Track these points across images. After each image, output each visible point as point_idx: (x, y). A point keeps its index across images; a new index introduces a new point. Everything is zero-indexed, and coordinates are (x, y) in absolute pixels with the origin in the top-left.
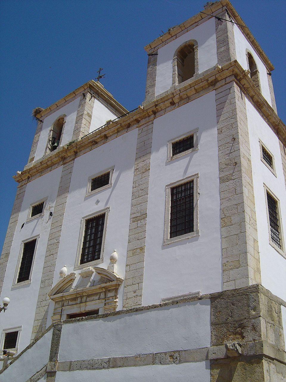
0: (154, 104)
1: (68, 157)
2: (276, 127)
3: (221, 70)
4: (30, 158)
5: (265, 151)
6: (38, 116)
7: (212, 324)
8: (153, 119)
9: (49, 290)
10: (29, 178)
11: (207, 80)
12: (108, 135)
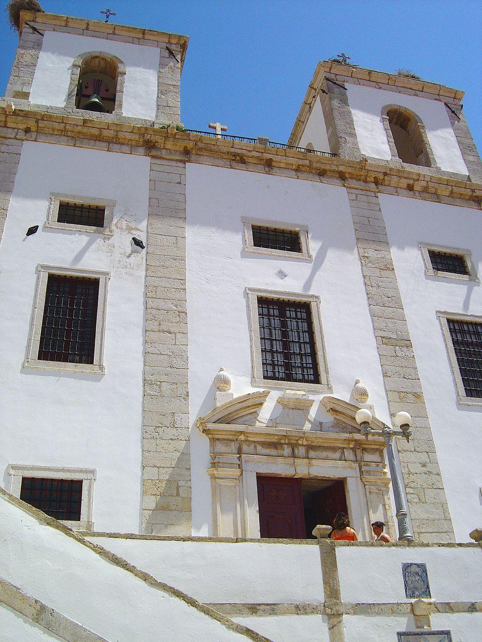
0: (384, 171)
10: (27, 131)
11: (473, 191)
12: (274, 164)
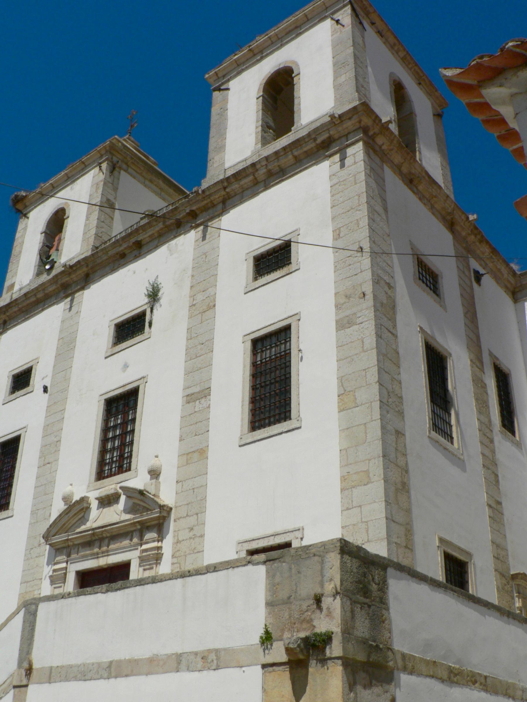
1: (73, 283)
2: (449, 218)
3: (339, 121)
4: (7, 284)
5: (423, 264)
6: (19, 206)
7: (269, 604)
8: (221, 211)
9: (44, 527)
